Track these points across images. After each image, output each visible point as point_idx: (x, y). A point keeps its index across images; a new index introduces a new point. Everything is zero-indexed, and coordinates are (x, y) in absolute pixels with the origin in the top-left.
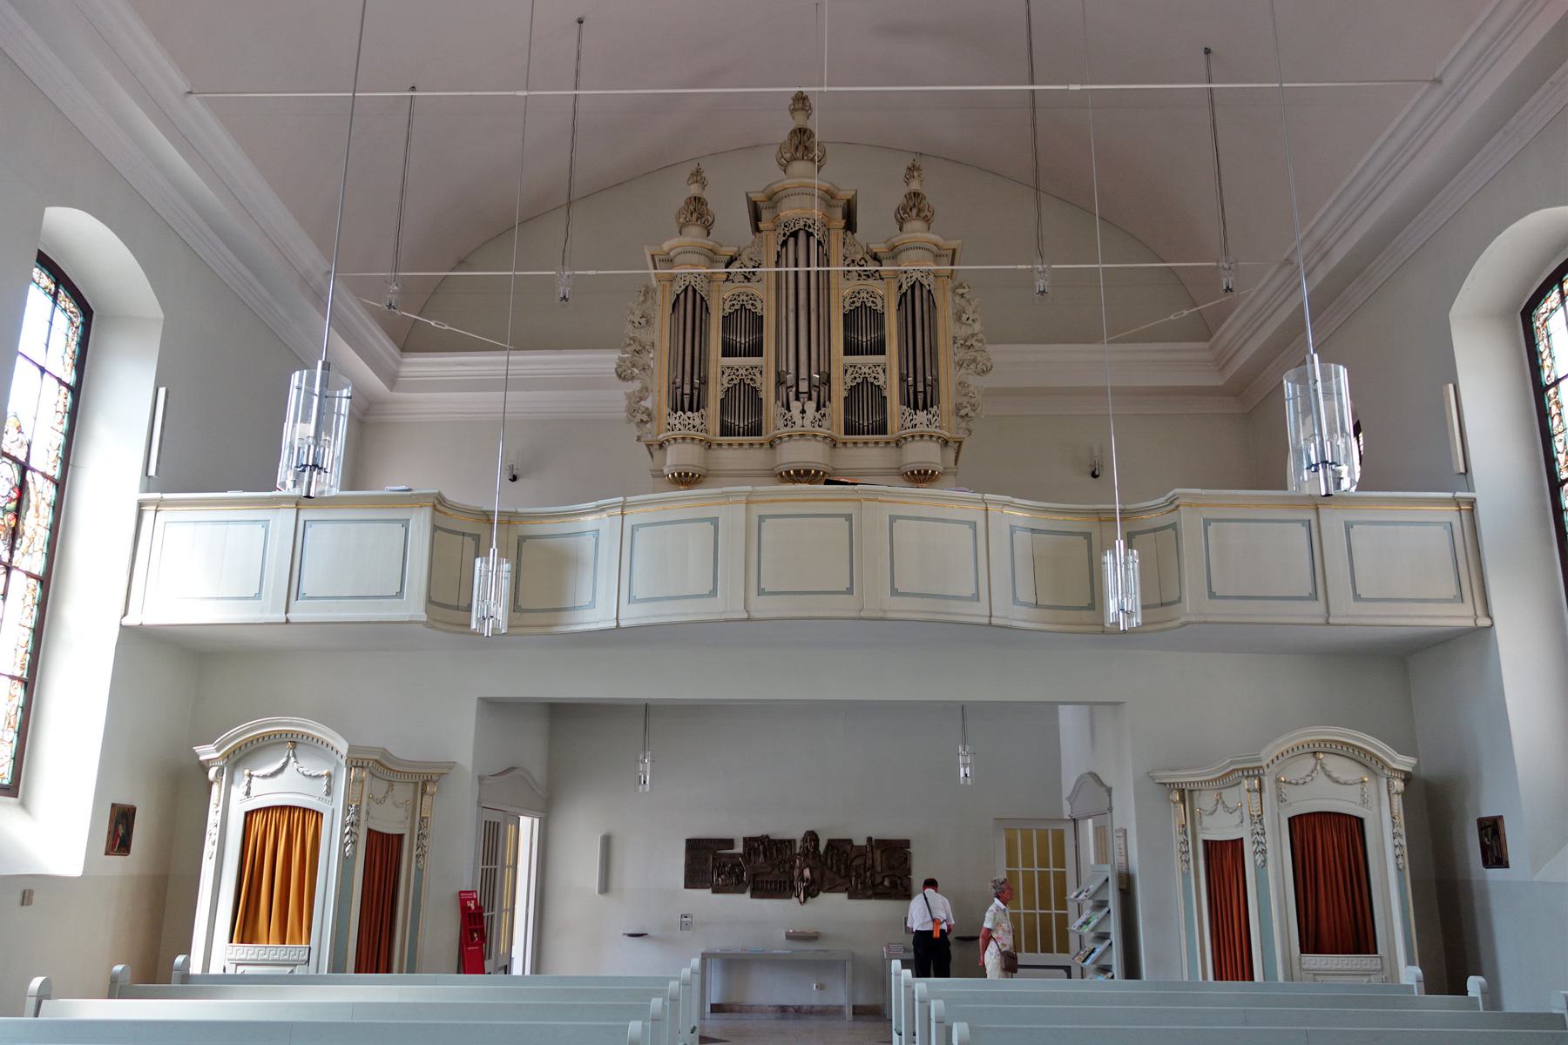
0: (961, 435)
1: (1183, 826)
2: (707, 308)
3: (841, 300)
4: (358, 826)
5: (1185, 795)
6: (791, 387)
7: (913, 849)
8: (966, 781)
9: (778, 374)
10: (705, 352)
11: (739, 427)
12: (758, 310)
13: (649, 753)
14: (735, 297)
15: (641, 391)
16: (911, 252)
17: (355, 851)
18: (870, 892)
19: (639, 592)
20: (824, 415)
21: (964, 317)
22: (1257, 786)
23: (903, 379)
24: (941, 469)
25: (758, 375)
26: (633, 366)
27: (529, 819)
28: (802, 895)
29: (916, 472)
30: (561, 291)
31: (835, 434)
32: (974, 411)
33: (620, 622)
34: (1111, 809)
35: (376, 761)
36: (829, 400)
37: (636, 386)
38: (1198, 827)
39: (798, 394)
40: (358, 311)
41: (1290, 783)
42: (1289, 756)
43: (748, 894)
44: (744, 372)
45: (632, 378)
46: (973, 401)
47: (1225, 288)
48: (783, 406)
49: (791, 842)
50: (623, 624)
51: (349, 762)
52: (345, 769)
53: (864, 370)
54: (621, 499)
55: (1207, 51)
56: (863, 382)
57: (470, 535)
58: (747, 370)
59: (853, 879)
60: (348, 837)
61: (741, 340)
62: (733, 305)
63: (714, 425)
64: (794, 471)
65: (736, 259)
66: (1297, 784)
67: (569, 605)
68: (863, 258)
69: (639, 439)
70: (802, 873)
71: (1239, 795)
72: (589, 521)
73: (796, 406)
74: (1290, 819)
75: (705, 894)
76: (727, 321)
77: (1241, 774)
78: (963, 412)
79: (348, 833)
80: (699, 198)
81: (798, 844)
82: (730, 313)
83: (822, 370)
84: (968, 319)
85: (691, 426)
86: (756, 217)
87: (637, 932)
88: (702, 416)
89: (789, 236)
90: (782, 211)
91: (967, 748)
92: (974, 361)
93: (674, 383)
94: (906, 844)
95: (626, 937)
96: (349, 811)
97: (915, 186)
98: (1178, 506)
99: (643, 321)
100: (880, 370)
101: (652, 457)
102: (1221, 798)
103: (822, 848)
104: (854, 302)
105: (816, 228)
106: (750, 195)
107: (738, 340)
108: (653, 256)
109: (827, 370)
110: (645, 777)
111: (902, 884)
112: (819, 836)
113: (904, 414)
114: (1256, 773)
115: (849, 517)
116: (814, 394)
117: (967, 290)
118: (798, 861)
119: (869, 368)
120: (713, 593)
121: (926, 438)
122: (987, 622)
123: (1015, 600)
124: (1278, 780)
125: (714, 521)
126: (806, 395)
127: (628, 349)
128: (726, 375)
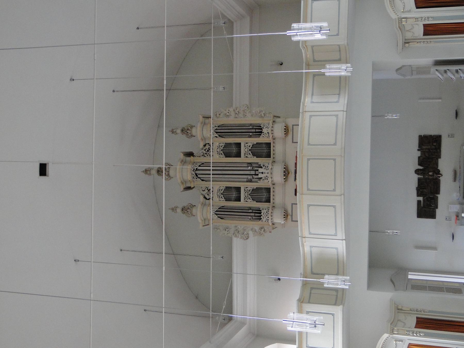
0: (272, 116)
1: (418, 43)
2: (223, 207)
3: (220, 158)
4: (414, 331)
5: (407, 42)
6: (253, 177)
7: (422, 134)
8: (398, 116)
9: (247, 181)
10: (238, 208)
11: (267, 196)
12: (223, 188)
13: (386, 231)
14: (219, 197)
15: (253, 232)
16: (204, 133)
17: (423, 332)
18: (439, 150)
19: (333, 232)
20: (263, 165)
21: (228, 114)
22: (405, 20)
23: (250, 137)
24: (284, 123)
25: (247, 189)
26: (243, 234)
27: (320, 332)
28: (439, 175)
29: (285, 133)
30: (220, 258)
31: (271, 162)
32: (262, 111)
33: (343, 239)
34: (410, 66)
35: (391, 324)
36: (258, 163)
37: (251, 233)
38: (418, 37)
39: (255, 175)
40: (335, 286)
41: (404, 8)
42: (394, 8)
43: (438, 195)
44: (246, 194)
45: (248, 234)
46: (259, 111)
47: (224, 24)
48: (260, 180)
49: (419, 180)
50: (344, 238)
51: (392, 334)
52: (394, 335)
53: (246, 151)
54: (300, 238)
55: (138, 28)
56: (251, 151)
57: (311, 291)
58: (246, 193)
59: (433, 156)
60: (418, 335)
61: (234, 195)
62: (221, 197)
63: (266, 205)
64: (284, 176)
65: (204, 196)
66: (404, 6)
67: (336, 257)
68: (205, 150)
69: (270, 232)
70: (431, 175)
71: (407, 25)
72: (307, 249)
73: (260, 176)
74: (417, 8)
75: (438, 212)
76: (227, 200)
77: (400, 25)
78: (263, 115)
79: (416, 334)
80: (182, 209)
81: (420, 176)
82: (224, 198)
83: (246, 166)
84: (228, 113)
85: (267, 213)
86: (189, 188)
87: (452, 237)
88: (263, 209)
89: (197, 177)
90: (188, 179)
91: (386, 115)
92: (244, 111)
93: (250, 219)
94: (421, 137)
95: (454, 241)
96: (408, 334)
97: (179, 131)
98: (306, 46)
99: (227, 230)
100: (246, 145)
101: (276, 227)
102: (408, 30)
103: (421, 168)
104: (221, 154)
105: (194, 167)
106: (181, 191)
107: (234, 196)
108: (203, 226)
109: (246, 164)
110: (395, 232)
111: (436, 138)
112: (417, 169)
113: (263, 137)
114: (400, 19)
115: (309, 160)
116: (256, 169)
117: (217, 113)
118: (426, 177)
119: (246, 148)
120: (334, 207)
121: (273, 129)
122: (345, 112)
123: (337, 102)
124: (403, 12)
125: (309, 206)
126: (256, 171)
127: (237, 236)
128: (247, 200)
